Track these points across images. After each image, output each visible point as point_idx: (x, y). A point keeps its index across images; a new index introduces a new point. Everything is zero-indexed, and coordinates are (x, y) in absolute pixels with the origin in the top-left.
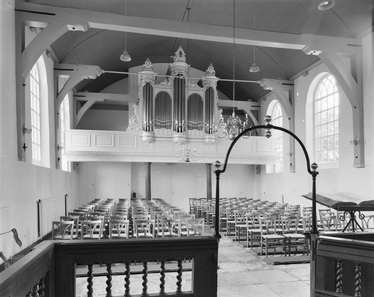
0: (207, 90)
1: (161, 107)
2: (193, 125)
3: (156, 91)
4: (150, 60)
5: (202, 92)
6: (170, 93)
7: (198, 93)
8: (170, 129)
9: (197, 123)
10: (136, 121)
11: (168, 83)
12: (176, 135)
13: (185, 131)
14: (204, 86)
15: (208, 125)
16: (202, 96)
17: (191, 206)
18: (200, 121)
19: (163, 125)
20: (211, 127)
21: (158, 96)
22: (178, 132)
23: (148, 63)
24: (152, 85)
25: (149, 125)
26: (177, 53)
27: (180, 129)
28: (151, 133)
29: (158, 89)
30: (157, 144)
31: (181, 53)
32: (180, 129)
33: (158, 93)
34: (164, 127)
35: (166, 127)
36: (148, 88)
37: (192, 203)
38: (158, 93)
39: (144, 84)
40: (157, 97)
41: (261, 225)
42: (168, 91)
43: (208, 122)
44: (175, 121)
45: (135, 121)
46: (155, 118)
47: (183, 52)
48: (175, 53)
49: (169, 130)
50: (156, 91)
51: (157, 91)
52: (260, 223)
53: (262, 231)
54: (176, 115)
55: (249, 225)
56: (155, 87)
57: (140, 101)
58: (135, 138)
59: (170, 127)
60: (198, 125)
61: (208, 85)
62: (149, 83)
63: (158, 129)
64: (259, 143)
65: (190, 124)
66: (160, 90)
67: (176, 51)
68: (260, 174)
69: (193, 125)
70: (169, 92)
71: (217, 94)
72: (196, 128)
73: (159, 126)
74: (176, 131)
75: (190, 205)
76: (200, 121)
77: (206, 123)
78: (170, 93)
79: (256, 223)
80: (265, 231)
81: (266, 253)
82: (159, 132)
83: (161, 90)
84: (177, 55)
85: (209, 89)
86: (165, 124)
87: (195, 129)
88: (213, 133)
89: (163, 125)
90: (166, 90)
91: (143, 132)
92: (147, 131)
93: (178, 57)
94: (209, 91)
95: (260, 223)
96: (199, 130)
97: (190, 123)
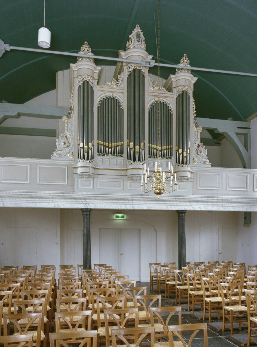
0: (179, 96)
1: (167, 120)
2: (107, 149)
3: (99, 94)
4: (88, 45)
5: (171, 100)
6: (121, 100)
7: (164, 100)
8: (121, 156)
9: (169, 146)
10: (67, 143)
11: (117, 84)
12: (131, 165)
13: (144, 160)
14: (174, 90)
15: (180, 151)
16: (171, 105)
17: (152, 274)
18: (167, 144)
19: (110, 150)
20: (185, 154)
21: (102, 104)
22: (135, 160)
23: (86, 49)
24: (91, 85)
25: (87, 150)
26: (133, 36)
27: (137, 156)
28: (91, 161)
29: (103, 93)
30: (101, 180)
31: (138, 36)
32: (137, 156)
33: (102, 100)
34: (111, 153)
35: (164, 156)
36: (86, 90)
37: (153, 271)
38: (102, 100)
39: (80, 84)
40: (100, 106)
41: (188, 282)
42: (118, 97)
43: (181, 146)
44: (79, 143)
45: (65, 143)
46: (149, 142)
47: (142, 35)
48: (130, 36)
49: (119, 158)
50: (99, 94)
51: (101, 96)
52: (188, 280)
53: (205, 293)
54: (80, 134)
55: (190, 286)
56: (98, 89)
57: (72, 112)
58: (27, 169)
59: (121, 153)
60: (167, 150)
61: (180, 88)
62: (88, 82)
63: (101, 157)
64: (228, 177)
65: (102, 147)
66: (105, 94)
67: (131, 33)
68: (249, 226)
69: (107, 149)
70: (119, 98)
71: (193, 103)
72: (111, 153)
73: (103, 152)
74: (81, 158)
75: (151, 273)
76: (167, 144)
77: (177, 147)
78: (121, 100)
79: (198, 284)
80: (207, 293)
81: (231, 329)
82: (103, 161)
83: (106, 95)
84: (133, 39)
85: (183, 94)
86: (113, 149)
87: (110, 155)
88: (188, 163)
89: (110, 150)
90: (114, 95)
91: (78, 161)
92: (84, 158)
93: (133, 42)
94: (182, 98)
95: (188, 280)
96: (166, 158)
97: (101, 144)
